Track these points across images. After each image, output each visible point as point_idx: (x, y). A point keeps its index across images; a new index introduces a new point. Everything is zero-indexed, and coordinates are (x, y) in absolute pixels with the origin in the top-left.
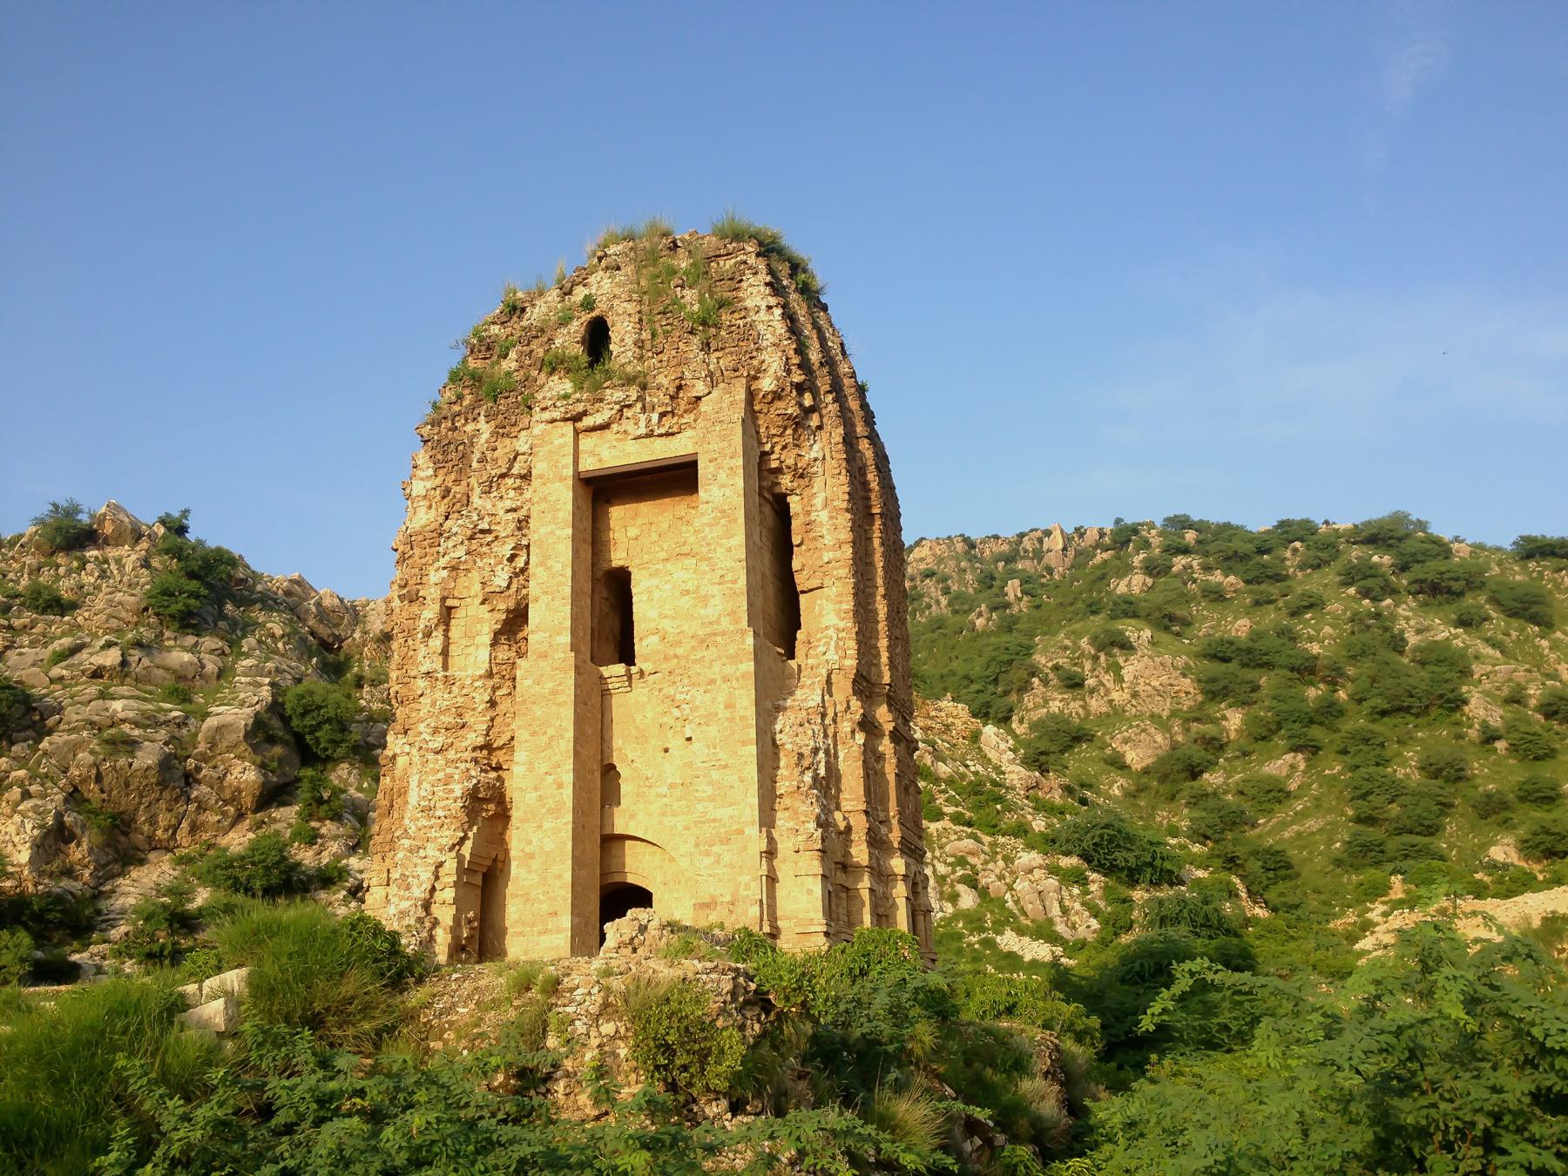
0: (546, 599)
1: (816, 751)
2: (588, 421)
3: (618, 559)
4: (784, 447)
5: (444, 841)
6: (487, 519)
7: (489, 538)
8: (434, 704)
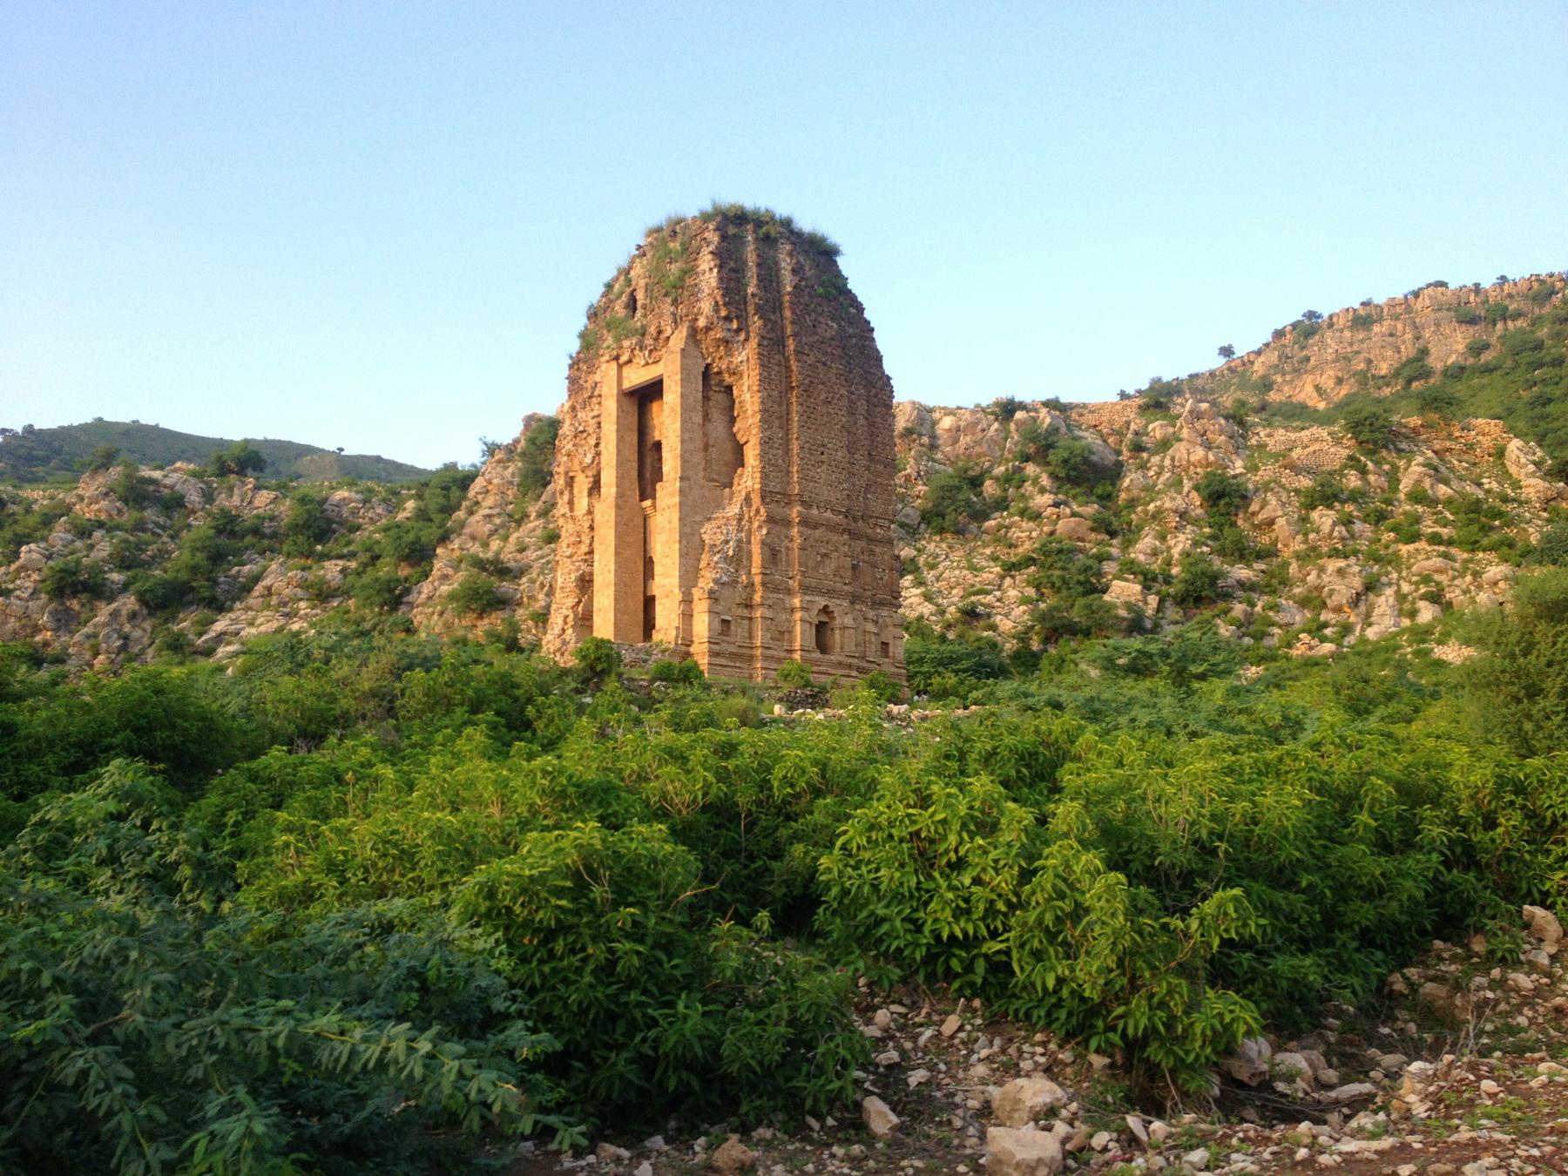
1: (727, 542)
2: (624, 359)
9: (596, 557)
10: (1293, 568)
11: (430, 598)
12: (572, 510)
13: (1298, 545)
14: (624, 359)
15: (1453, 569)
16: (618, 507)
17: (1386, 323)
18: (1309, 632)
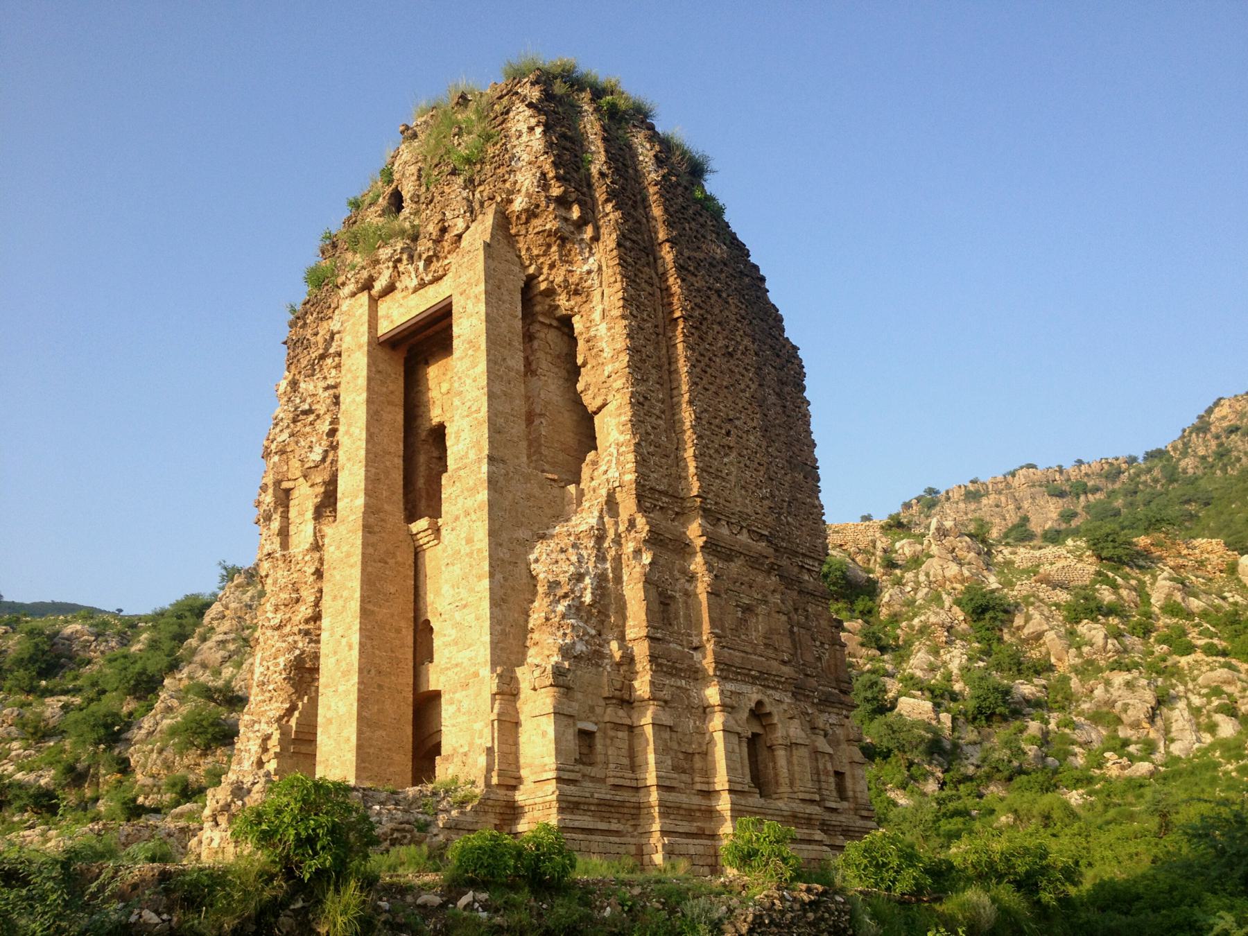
0: (349, 465)
1: (579, 577)
2: (379, 286)
3: (436, 415)
4: (552, 266)
5: (271, 714)
6: (309, 400)
7: (311, 417)
8: (275, 583)
9: (325, 622)
10: (1075, 683)
11: (150, 733)
12: (285, 545)
13: (1072, 658)
14: (379, 286)
15: (1239, 679)
16: (367, 529)
17: (992, 497)
18: (1114, 750)
